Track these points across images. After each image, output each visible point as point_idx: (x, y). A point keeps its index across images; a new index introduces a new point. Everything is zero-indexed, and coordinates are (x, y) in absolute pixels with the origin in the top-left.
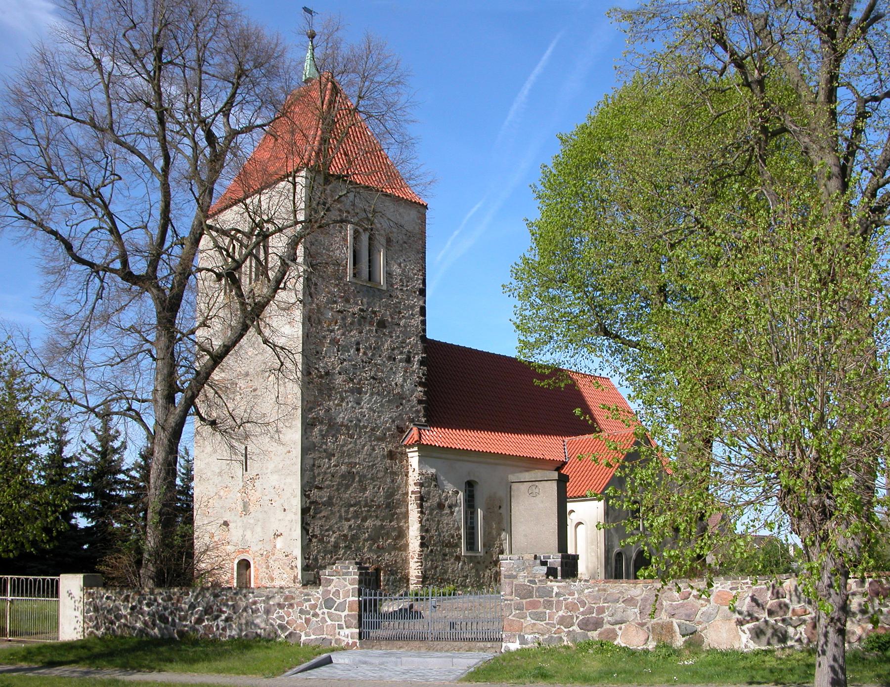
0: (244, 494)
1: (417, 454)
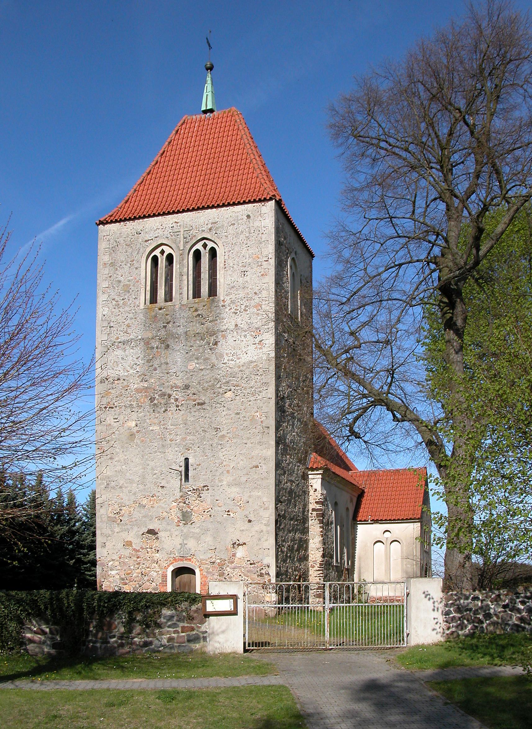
0: (182, 504)
1: (320, 476)
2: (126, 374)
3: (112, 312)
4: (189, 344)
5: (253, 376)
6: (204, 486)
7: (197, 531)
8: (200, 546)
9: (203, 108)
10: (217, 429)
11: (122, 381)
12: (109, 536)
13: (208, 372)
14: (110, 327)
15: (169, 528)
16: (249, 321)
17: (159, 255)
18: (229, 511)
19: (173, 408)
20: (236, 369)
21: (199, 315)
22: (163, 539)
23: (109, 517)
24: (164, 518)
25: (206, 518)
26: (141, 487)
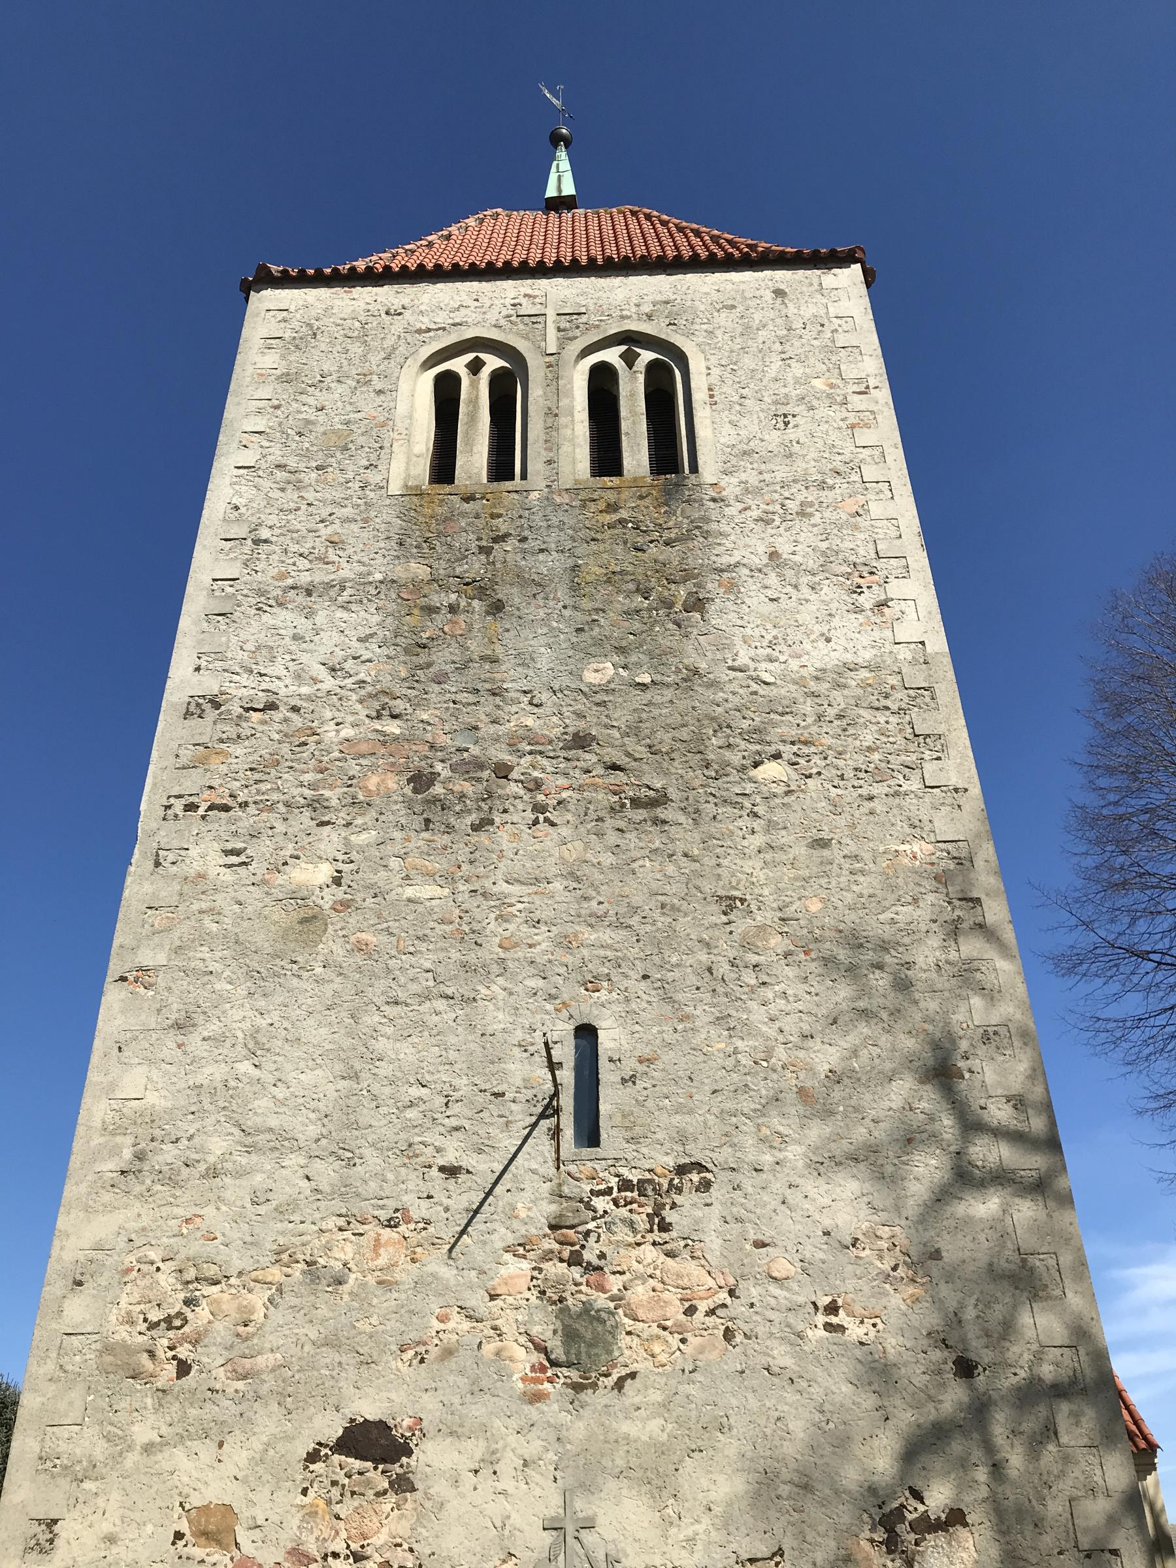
0: (556, 1269)
2: (305, 690)
3: (269, 501)
4: (586, 604)
5: (867, 714)
6: (681, 1170)
7: (652, 1428)
8: (678, 1534)
9: (551, 192)
10: (729, 903)
11: (284, 712)
12: (92, 1471)
13: (669, 694)
14: (257, 542)
15: (477, 1411)
16: (824, 545)
17: (463, 373)
18: (832, 1309)
19: (522, 815)
20: (785, 691)
21: (622, 522)
22: (440, 1488)
23: (108, 1349)
24: (448, 1353)
25: (701, 1350)
26: (327, 1172)
